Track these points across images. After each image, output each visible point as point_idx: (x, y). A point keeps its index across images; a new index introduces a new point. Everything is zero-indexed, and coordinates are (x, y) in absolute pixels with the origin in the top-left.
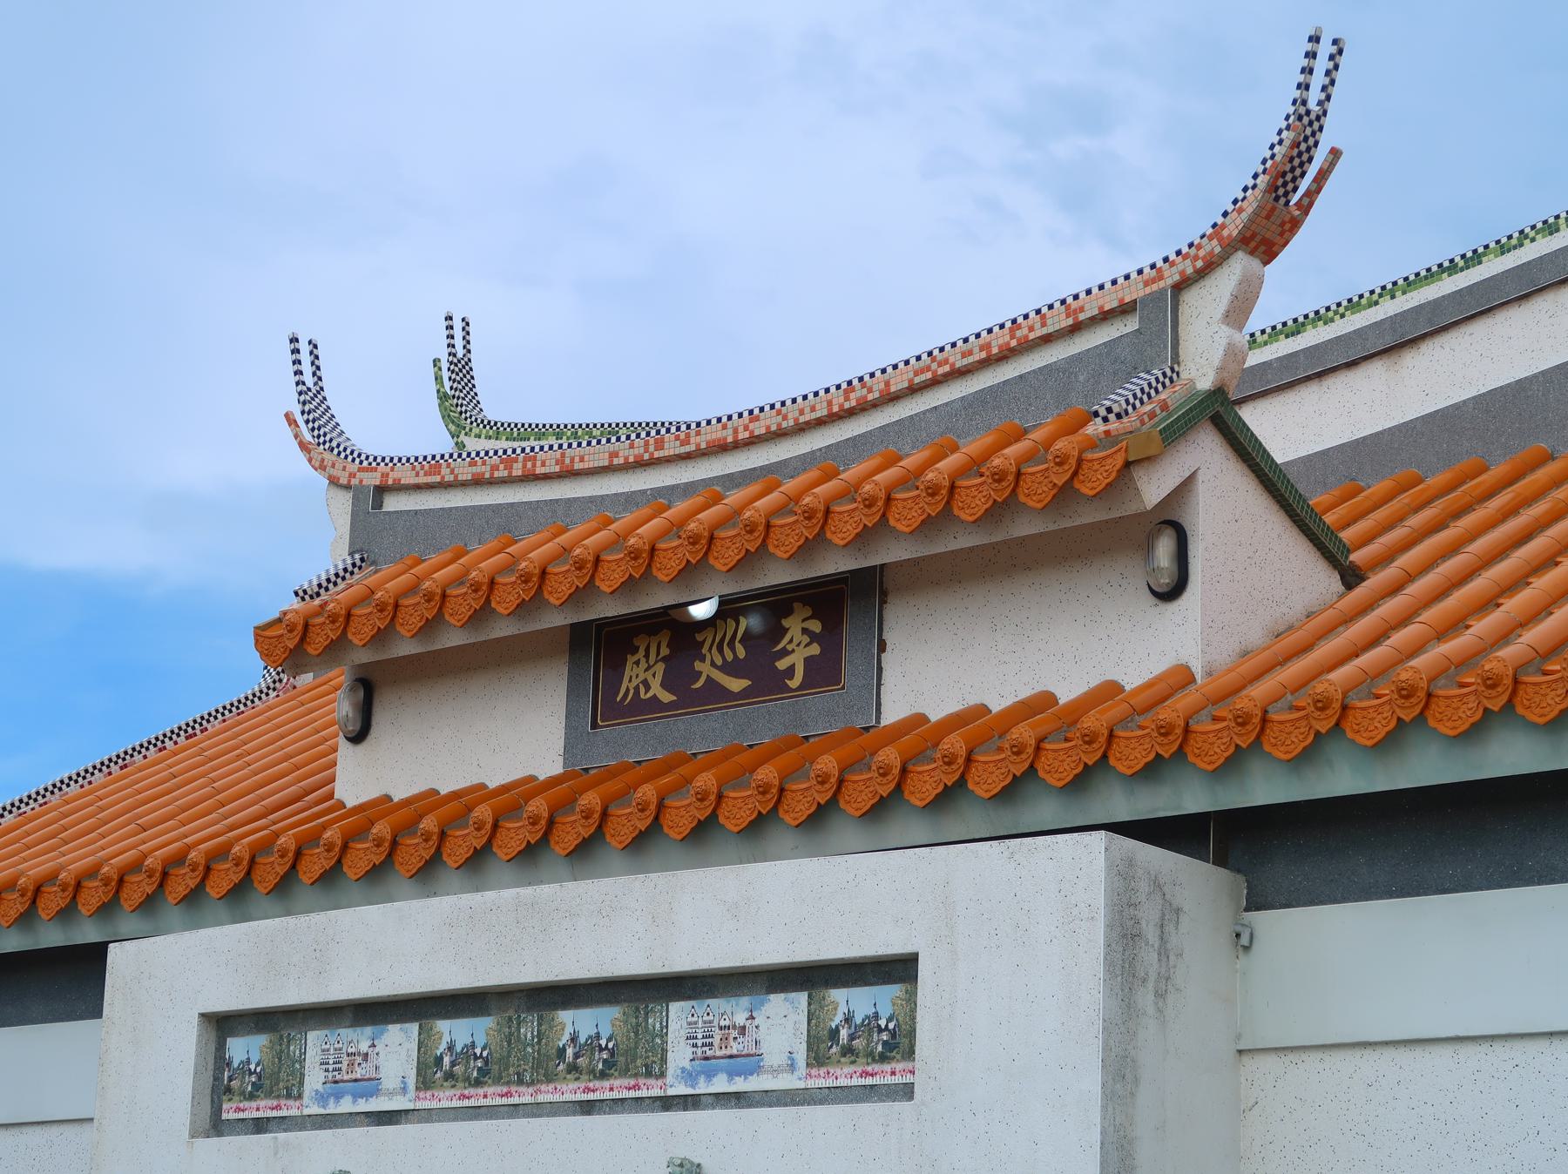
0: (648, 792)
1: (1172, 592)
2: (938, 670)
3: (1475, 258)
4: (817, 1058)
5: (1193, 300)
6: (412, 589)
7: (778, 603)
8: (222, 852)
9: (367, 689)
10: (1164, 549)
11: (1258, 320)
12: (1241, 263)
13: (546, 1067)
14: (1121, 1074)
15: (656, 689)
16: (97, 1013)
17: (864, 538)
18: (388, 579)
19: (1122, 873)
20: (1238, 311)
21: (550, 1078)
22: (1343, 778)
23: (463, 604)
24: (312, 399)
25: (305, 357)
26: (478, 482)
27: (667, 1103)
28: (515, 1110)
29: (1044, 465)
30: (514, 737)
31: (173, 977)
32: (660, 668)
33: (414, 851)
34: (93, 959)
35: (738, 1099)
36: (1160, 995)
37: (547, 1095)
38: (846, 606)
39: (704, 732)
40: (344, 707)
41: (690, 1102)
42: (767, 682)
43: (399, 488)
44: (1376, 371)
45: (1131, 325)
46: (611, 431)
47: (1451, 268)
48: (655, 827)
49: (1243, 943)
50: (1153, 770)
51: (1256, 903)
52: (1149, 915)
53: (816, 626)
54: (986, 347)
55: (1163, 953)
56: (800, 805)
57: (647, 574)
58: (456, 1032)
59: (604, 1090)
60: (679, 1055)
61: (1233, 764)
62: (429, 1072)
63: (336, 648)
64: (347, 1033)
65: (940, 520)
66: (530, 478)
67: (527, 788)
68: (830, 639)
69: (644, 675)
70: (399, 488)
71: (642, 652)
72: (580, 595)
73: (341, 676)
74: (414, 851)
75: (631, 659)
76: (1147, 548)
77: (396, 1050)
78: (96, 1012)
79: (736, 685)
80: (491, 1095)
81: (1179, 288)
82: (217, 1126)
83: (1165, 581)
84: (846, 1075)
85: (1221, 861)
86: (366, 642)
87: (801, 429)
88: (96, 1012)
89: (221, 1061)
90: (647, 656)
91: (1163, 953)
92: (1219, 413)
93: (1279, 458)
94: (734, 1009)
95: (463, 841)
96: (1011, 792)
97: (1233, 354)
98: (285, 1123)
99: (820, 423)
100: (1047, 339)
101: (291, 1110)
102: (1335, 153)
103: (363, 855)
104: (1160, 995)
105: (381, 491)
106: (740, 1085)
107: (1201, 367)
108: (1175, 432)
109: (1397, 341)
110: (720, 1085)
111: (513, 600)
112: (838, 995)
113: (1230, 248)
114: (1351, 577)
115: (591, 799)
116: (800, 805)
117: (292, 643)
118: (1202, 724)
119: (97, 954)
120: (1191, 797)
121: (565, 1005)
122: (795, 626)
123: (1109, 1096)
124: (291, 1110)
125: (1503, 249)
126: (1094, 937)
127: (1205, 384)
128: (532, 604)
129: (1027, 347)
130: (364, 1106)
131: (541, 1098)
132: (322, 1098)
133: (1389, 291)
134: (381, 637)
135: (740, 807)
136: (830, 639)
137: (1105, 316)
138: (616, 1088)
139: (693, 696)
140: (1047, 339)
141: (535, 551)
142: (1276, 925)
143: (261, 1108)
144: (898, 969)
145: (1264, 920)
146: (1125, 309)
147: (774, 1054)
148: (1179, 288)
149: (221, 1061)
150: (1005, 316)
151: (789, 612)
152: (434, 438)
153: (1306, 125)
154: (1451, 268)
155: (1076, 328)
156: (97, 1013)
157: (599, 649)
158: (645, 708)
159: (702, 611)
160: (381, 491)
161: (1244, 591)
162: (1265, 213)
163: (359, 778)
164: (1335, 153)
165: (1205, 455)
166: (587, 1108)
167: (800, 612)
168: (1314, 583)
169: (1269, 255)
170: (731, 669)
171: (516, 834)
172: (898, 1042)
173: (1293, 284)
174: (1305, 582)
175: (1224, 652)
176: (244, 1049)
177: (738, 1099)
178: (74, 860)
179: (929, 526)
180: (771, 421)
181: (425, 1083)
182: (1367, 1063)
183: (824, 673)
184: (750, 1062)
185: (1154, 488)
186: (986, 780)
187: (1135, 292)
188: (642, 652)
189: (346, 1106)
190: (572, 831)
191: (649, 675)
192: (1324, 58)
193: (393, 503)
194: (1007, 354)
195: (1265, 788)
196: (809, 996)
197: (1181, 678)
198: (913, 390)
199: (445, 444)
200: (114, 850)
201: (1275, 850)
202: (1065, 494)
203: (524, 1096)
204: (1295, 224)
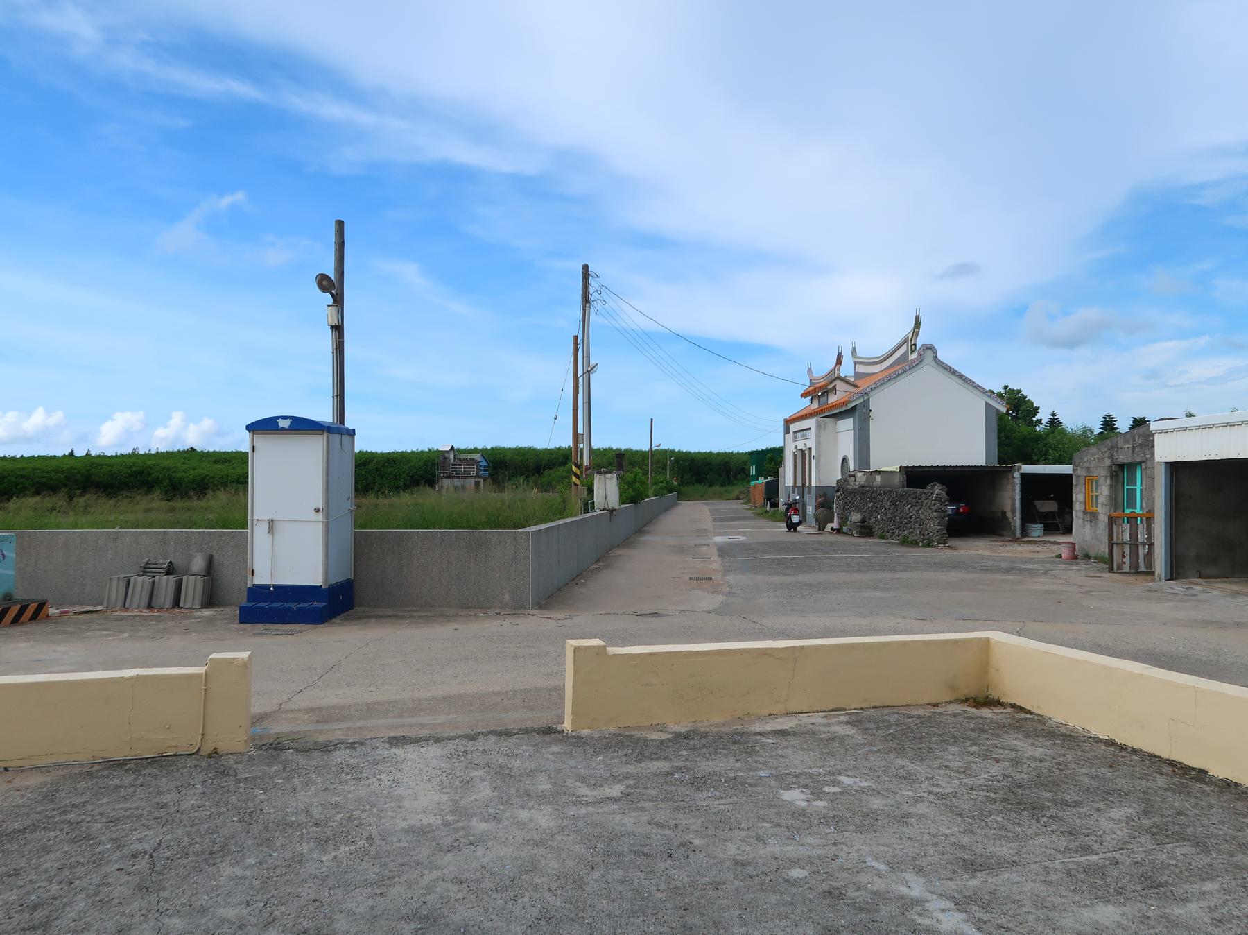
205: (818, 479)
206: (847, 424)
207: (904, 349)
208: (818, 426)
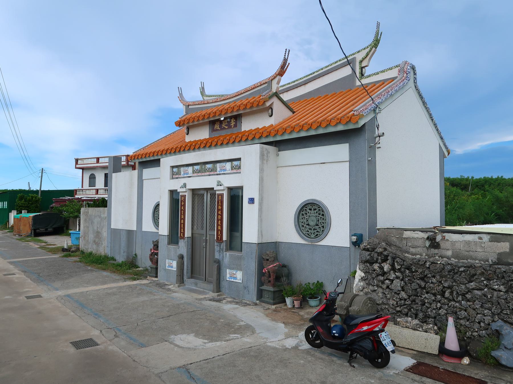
0: (216, 140)
1: (271, 116)
2: (248, 125)
3: (314, 73)
4: (232, 169)
5: (273, 81)
6: (229, 107)
7: (231, 117)
8: (173, 148)
9: (188, 129)
10: (270, 111)
11: (281, 84)
12: (278, 77)
14: (262, 170)
17: (238, 110)
18: (188, 116)
19: (262, 149)
20: (278, 83)
22: (286, 137)
23: (196, 119)
24: (181, 95)
25: (180, 90)
26: (199, 104)
27: (217, 174)
28: (202, 176)
29: (257, 101)
30: (203, 134)
31: (167, 162)
33: (192, 147)
34: (159, 160)
35: (224, 174)
36: (267, 161)
37: (205, 174)
38: (238, 118)
39: (223, 133)
40: (186, 131)
41: (220, 174)
42: (230, 127)
43: (190, 105)
44: (303, 87)
45: (266, 85)
46: (222, 96)
47: (311, 74)
48: (195, 148)
49: (278, 155)
50: (267, 136)
51: (279, 151)
52: (265, 153)
55: (267, 157)
56: (231, 141)
57: (252, 106)
58: (196, 167)
59: (211, 173)
60: (218, 169)
61: (275, 136)
62: (194, 172)
63: (183, 124)
64: (222, 164)
65: (245, 108)
66: (204, 104)
67: (205, 139)
68: (236, 122)
69: (217, 127)
70: (190, 105)
72: (209, 118)
73: (185, 127)
74: (192, 147)
76: (268, 111)
77: (190, 169)
79: (226, 127)
80: (200, 174)
81: (272, 80)
82: (173, 178)
83: (270, 114)
84: (235, 171)
85: (275, 146)
86: (188, 123)
87: (232, 97)
89: (173, 171)
91: (267, 157)
92: (276, 95)
93: (285, 100)
94: (223, 164)
95: (197, 146)
96: (253, 139)
97: (278, 88)
98: (180, 178)
99: (234, 97)
100: (258, 86)
101: (180, 176)
102: (289, 64)
103: (187, 148)
104: (267, 161)
105: (188, 105)
106: (224, 172)
107: (274, 90)
108: (271, 97)
109: (305, 83)
110: (222, 172)
111: (243, 108)
112: (234, 162)
113: (277, 75)
114: (294, 112)
115: (228, 138)
116: (231, 141)
117: (179, 124)
118: (272, 131)
119: (159, 160)
120: (271, 139)
122: (232, 120)
123: (260, 173)
124: (180, 176)
125: (317, 72)
126: (258, 155)
127: (274, 92)
128: (203, 119)
129: (256, 87)
133: (304, 77)
134: (188, 123)
135: (225, 141)
136: (236, 122)
137: (264, 84)
138: (212, 173)
139: (222, 129)
140: (258, 86)
141: (209, 111)
142: (281, 153)
143: (177, 176)
144: (239, 159)
145: (280, 153)
146: (266, 83)
147: (228, 169)
148: (272, 80)
149: (173, 171)
152: (200, 98)
153: (285, 60)
154: (311, 74)
155: (261, 85)
157: (212, 123)
158: (224, 128)
159: (222, 119)
160: (188, 105)
161: (280, 115)
162: (281, 71)
163: (188, 139)
164: (289, 64)
165: (275, 100)
166: (209, 175)
167: (233, 119)
168: (289, 114)
169: (282, 76)
170: (226, 125)
171: (203, 145)
172: (239, 168)
173: (285, 80)
174: (288, 114)
175: (277, 122)
176: (175, 170)
177: (224, 174)
178: (157, 149)
179: (244, 109)
180: (229, 97)
181: (193, 173)
182: (287, 168)
183: (235, 126)
184: (225, 170)
185: (268, 104)
186: (250, 138)
187: (267, 81)
189: (185, 176)
190: (208, 145)
192: (287, 52)
193: (190, 107)
194: (254, 88)
195: (279, 138)
196: (350, 145)
197: (272, 125)
198: (244, 93)
199: (202, 99)
200: (161, 148)
201: (280, 145)
202: (258, 105)
203: (203, 174)
204: (285, 72)
205: (261, 233)
206: (341, 151)
207: (347, 71)
208: (263, 156)
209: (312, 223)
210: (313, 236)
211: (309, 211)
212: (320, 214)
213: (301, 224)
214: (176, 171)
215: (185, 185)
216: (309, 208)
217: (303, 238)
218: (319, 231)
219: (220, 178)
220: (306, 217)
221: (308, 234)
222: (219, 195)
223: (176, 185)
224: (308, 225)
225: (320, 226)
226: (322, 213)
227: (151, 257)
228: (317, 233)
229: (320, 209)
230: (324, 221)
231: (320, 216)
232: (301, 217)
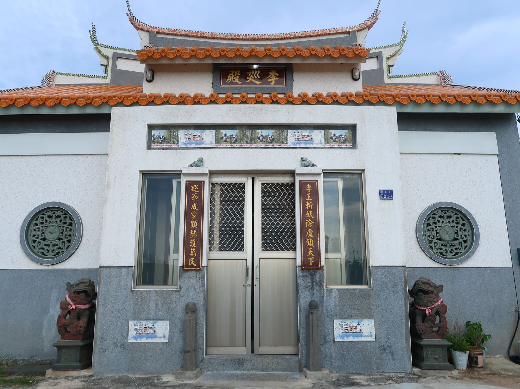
13: (254, 140)
15: (237, 81)
16: (108, 131)
21: (255, 143)
32: (238, 77)
53: (277, 75)
54: (318, 33)
62: (218, 140)
71: (232, 74)
75: (230, 75)
78: (108, 131)
80: (166, 145)
88: (108, 131)
90: (234, 74)
94: (307, 132)
100: (329, 34)
106: (308, 146)
110: (303, 146)
121: (259, 129)
124: (176, 146)
130: (198, 146)
131: (253, 146)
132: (184, 144)
146: (349, 33)
150: (322, 29)
151: (271, 71)
156: (108, 131)
188: (232, 74)
191: (235, 78)
198: (300, 37)
209: (446, 237)
210: (449, 255)
211: (47, 219)
212: (65, 223)
213: (31, 239)
214: (162, 135)
215: (200, 163)
216: (48, 214)
217: (33, 259)
218: (460, 247)
219: (309, 155)
220: (41, 228)
221: (43, 253)
222: (304, 184)
223: (162, 161)
224: (44, 239)
225: (461, 240)
226: (68, 221)
227: (63, 321)
228: (456, 251)
229: (68, 216)
230: (71, 233)
231: (66, 226)
232: (33, 227)
